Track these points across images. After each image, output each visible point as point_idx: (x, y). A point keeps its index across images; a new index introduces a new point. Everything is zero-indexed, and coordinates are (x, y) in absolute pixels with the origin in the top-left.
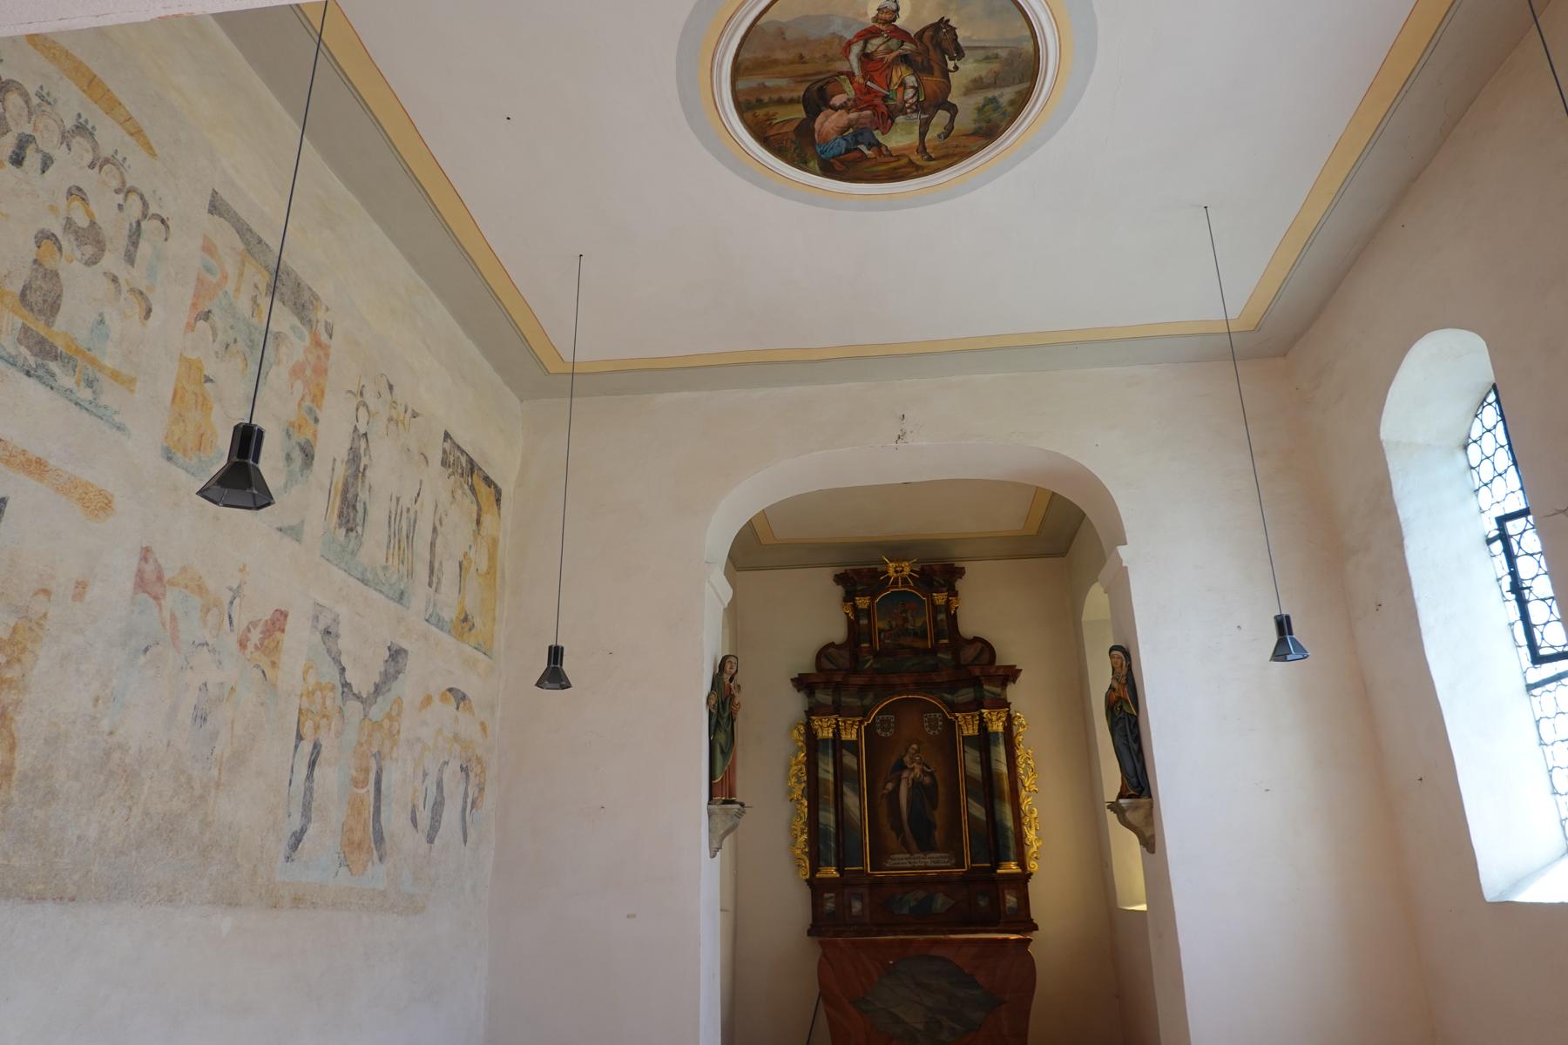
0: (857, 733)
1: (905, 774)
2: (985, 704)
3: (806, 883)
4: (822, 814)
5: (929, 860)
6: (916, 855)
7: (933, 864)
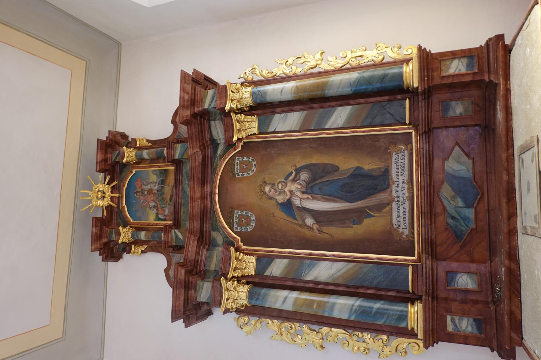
0: (250, 255)
1: (297, 202)
2: (221, 106)
3: (430, 348)
4: (336, 314)
5: (401, 178)
6: (394, 195)
7: (406, 173)
